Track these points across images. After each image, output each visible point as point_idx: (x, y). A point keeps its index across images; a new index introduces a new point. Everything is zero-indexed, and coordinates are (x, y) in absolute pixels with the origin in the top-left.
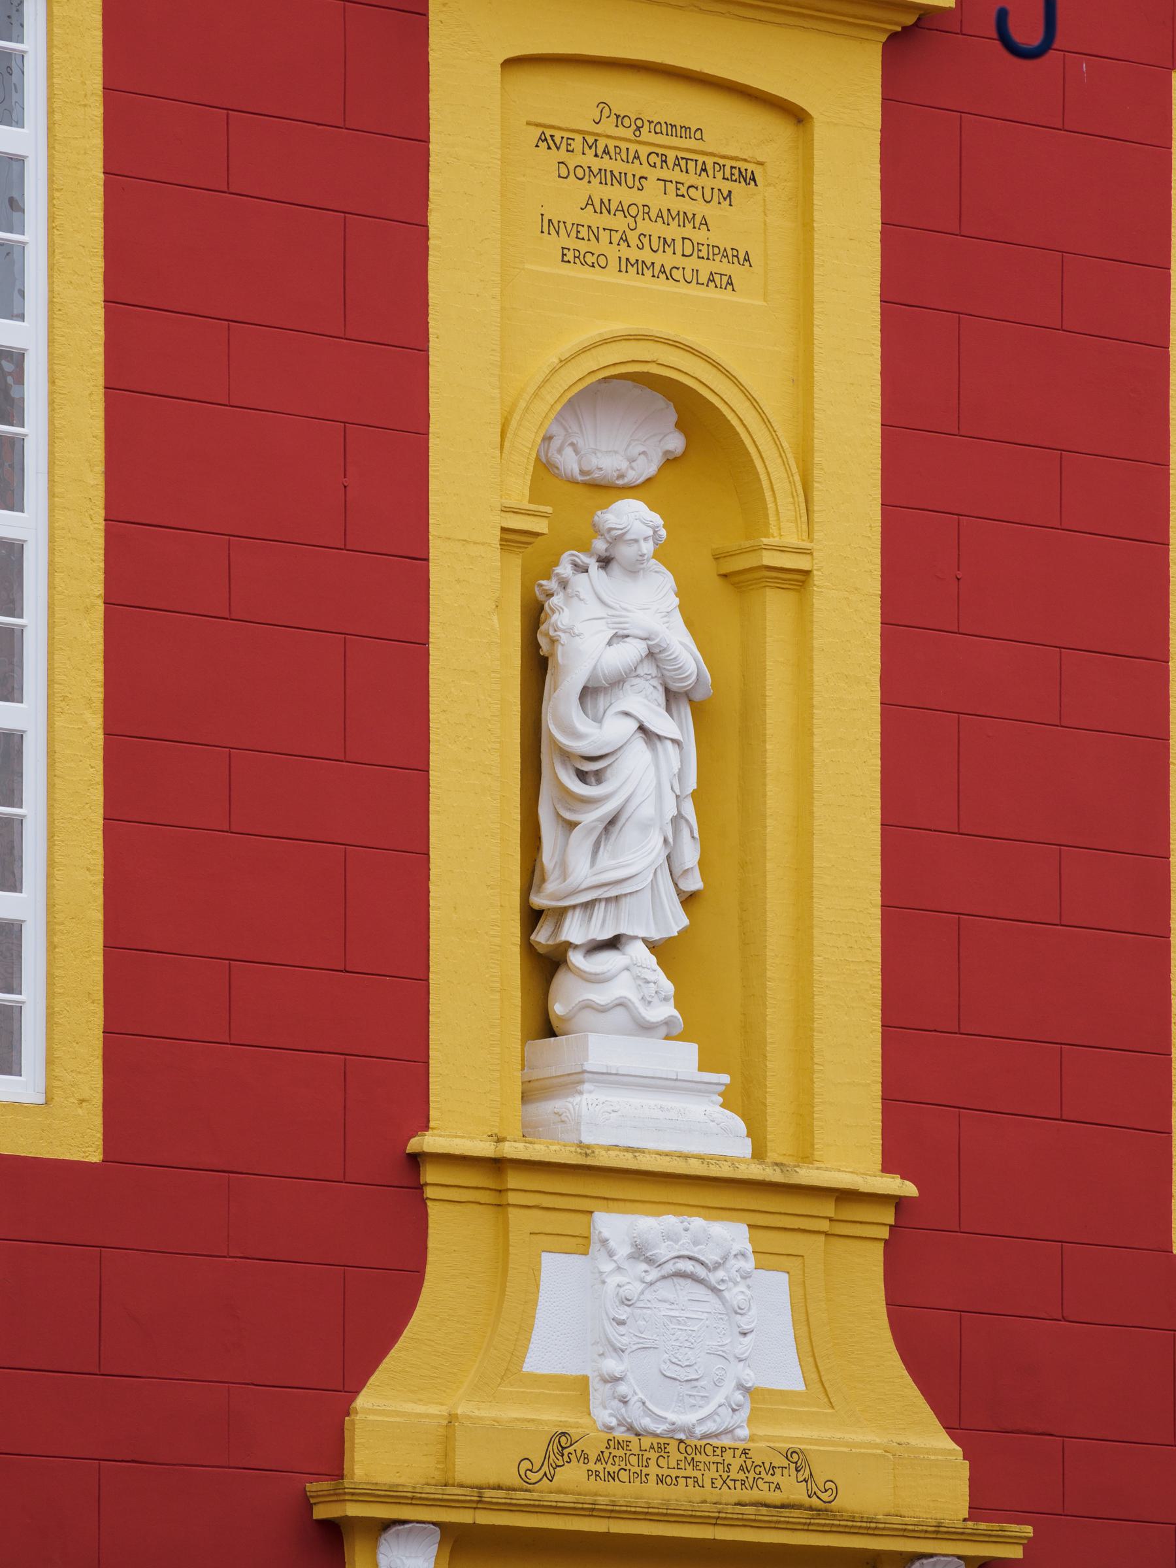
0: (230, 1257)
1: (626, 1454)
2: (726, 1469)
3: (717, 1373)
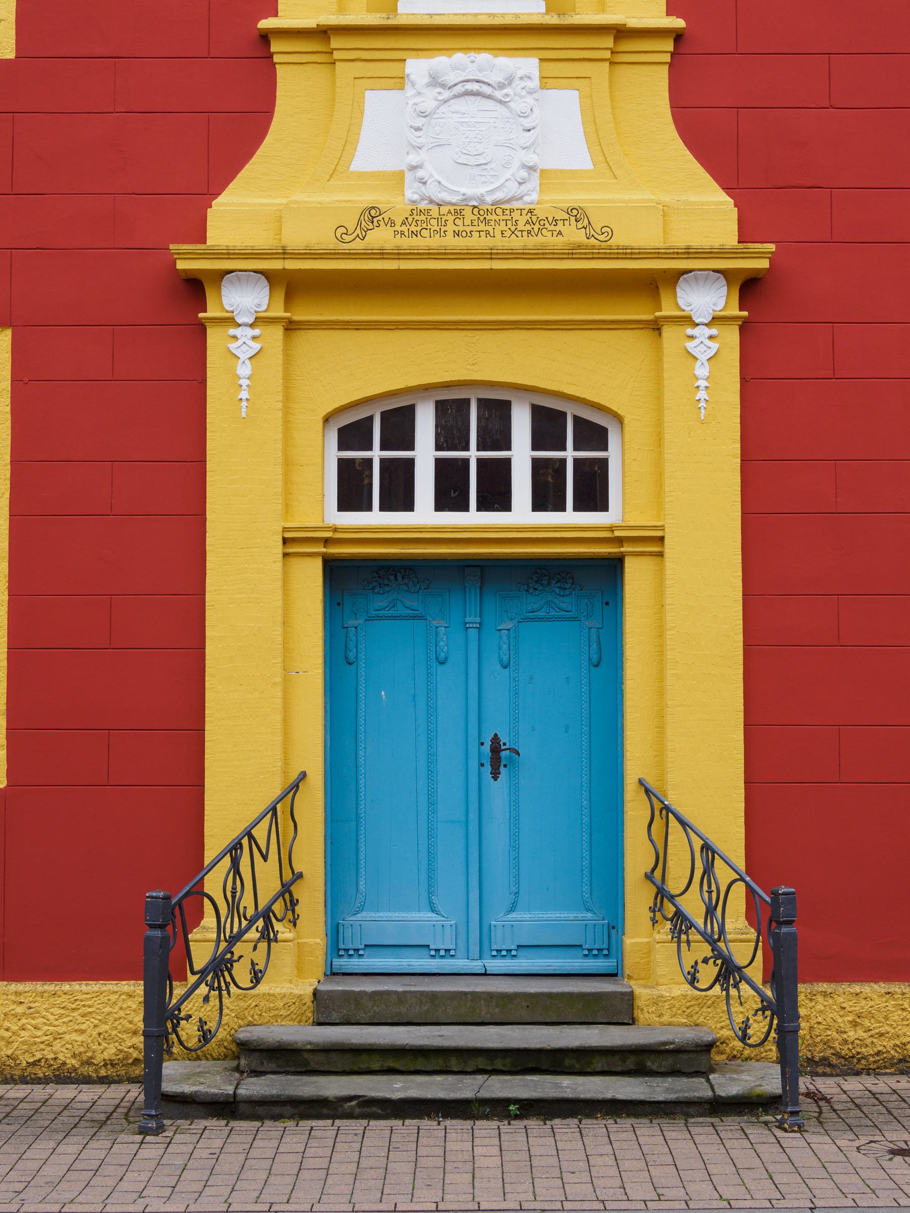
0: (117, 113)
1: (427, 218)
2: (514, 223)
3: (505, 158)
